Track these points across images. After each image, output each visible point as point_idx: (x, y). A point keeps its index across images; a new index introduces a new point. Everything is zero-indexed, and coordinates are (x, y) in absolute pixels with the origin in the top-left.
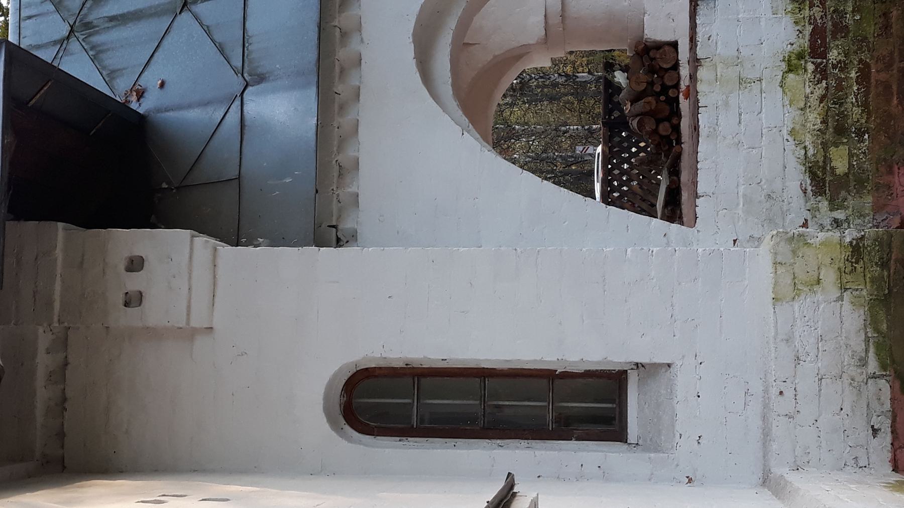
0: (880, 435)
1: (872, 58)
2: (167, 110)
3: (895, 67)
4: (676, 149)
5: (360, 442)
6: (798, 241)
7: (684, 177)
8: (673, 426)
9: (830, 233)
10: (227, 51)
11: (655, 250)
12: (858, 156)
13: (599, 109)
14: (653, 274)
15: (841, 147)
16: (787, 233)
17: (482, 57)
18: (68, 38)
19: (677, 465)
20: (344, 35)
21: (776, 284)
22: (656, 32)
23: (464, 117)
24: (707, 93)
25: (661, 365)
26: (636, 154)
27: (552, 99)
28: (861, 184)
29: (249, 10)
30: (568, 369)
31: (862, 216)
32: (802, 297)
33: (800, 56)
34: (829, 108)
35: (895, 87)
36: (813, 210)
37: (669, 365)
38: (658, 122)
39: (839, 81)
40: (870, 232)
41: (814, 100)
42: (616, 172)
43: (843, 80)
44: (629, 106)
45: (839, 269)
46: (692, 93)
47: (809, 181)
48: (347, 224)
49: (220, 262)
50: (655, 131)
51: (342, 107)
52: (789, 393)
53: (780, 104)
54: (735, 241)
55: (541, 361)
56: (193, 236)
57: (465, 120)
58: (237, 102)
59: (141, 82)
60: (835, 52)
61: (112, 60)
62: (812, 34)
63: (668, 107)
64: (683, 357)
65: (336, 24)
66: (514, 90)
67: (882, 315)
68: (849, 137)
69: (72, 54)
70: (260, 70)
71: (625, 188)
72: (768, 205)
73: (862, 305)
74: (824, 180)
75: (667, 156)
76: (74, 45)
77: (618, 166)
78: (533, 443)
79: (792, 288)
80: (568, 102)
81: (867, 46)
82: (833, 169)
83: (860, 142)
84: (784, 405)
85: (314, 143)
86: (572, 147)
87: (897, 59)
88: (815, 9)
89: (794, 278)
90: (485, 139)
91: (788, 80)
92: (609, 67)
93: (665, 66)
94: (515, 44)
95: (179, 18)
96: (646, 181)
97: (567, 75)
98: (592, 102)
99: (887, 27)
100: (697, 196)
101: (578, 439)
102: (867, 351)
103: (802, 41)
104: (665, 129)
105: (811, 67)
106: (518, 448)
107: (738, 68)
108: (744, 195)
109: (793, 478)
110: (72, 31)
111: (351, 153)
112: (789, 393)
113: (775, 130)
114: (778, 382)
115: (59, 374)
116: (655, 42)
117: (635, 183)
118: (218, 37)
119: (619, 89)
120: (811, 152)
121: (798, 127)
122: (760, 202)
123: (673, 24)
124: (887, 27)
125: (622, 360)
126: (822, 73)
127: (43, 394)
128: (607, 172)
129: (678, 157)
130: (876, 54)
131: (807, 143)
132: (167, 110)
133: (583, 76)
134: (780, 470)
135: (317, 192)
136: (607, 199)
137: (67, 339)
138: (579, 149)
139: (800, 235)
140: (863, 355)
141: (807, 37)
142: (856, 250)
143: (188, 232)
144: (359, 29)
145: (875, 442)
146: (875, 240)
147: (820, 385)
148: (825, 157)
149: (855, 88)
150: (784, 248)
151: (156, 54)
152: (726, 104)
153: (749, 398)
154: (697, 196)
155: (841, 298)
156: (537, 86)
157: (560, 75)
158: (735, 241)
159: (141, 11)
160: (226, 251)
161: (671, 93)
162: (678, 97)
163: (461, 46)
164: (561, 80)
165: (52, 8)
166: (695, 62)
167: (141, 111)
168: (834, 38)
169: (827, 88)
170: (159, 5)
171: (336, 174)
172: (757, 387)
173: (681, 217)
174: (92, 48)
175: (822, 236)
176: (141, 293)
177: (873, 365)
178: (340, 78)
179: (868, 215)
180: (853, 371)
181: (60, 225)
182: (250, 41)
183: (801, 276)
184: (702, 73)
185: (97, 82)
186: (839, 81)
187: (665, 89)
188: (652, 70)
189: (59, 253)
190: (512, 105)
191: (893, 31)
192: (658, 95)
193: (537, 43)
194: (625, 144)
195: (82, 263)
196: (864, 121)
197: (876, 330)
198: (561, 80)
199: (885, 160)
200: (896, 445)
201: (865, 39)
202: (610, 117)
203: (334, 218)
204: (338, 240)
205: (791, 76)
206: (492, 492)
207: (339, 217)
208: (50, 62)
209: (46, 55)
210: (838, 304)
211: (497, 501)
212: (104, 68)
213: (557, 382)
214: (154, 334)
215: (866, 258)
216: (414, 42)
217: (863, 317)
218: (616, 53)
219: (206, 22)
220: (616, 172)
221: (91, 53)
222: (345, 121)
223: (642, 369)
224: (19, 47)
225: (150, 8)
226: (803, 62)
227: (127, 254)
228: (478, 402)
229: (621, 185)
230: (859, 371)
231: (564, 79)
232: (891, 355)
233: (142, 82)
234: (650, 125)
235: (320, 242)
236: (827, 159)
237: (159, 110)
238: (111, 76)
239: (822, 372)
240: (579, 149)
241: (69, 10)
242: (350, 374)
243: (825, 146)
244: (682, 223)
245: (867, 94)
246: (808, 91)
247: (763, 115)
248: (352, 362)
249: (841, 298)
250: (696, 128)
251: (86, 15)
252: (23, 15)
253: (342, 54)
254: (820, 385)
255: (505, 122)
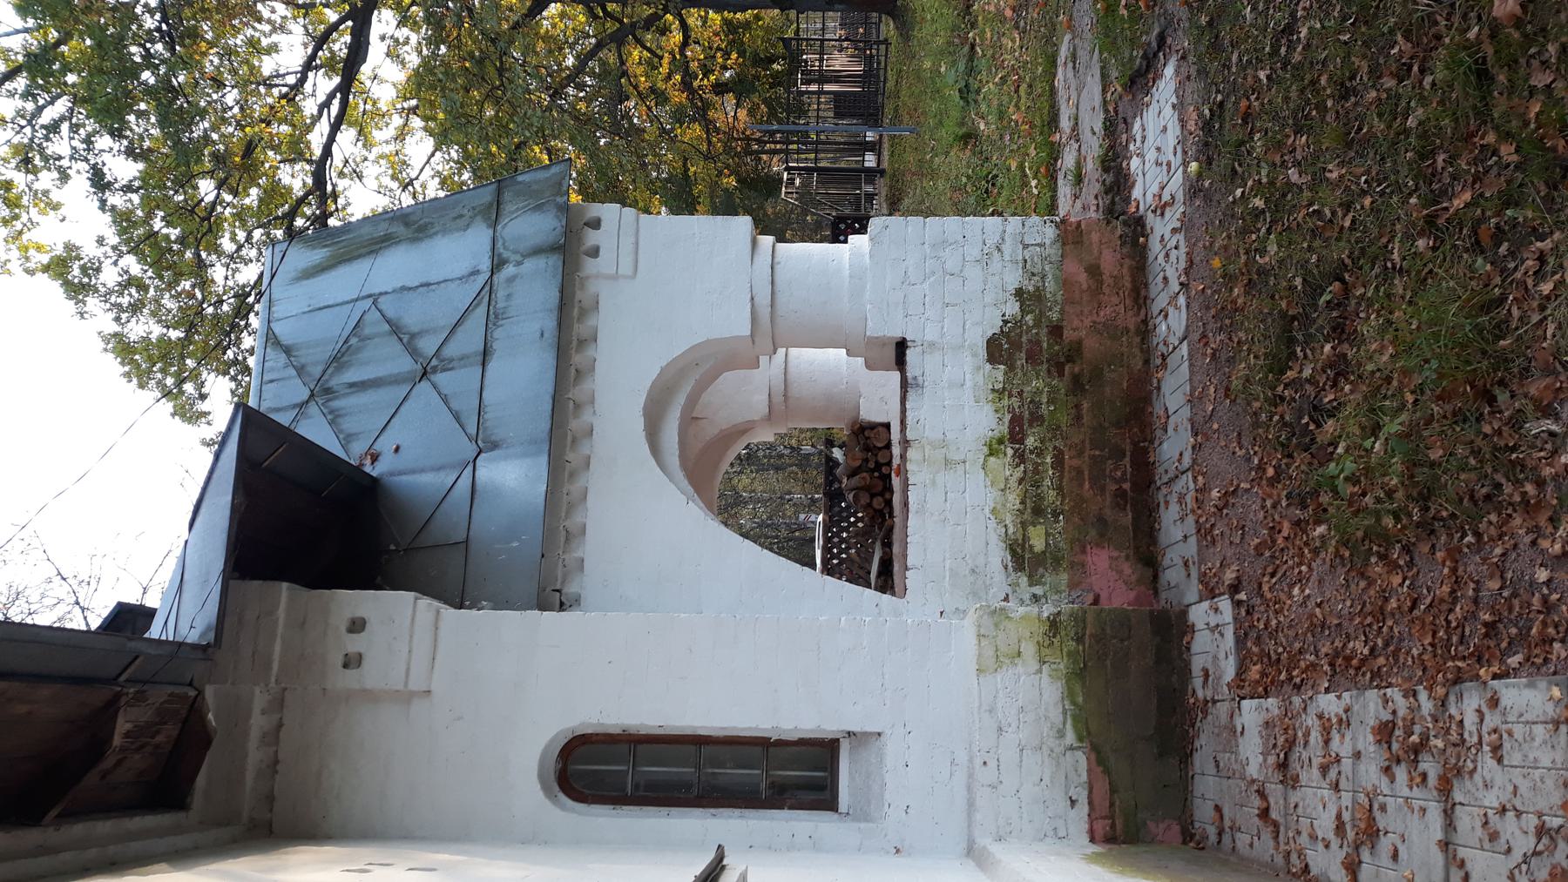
0: (1077, 806)
1: (1065, 446)
2: (401, 473)
3: (1086, 454)
4: (888, 522)
5: (573, 810)
6: (1000, 615)
7: (896, 549)
8: (883, 796)
9: (1029, 608)
10: (463, 420)
11: (867, 620)
12: (1054, 536)
13: (821, 480)
14: (864, 644)
15: (1039, 527)
16: (989, 607)
17: (710, 431)
18: (307, 402)
19: (886, 836)
20: (577, 406)
21: (980, 655)
22: (872, 412)
23: (690, 487)
24: (918, 473)
25: (871, 734)
26: (855, 524)
27: (777, 469)
28: (1057, 562)
29: (486, 382)
30: (783, 737)
31: (1058, 592)
32: (1004, 668)
33: (1000, 441)
34: (1027, 490)
35: (1086, 473)
36: (1014, 585)
37: (879, 734)
38: (873, 496)
39: (1037, 465)
40: (1066, 607)
41: (1013, 483)
42: (836, 540)
43: (1039, 464)
44: (845, 480)
45: (1038, 642)
46: (902, 471)
47: (1009, 558)
48: (571, 589)
49: (443, 626)
50: (869, 505)
51: (572, 475)
52: (992, 764)
53: (982, 484)
54: (942, 613)
55: (756, 729)
56: (416, 599)
57: (690, 489)
58: (470, 468)
59: (374, 447)
60: (1032, 439)
61: (348, 425)
62: (1011, 421)
63: (881, 483)
64: (893, 726)
65: (570, 396)
66: (741, 460)
67: (1078, 688)
68: (1045, 517)
69: (310, 417)
70: (493, 438)
71: (844, 556)
72: (972, 579)
73: (1059, 678)
74: (1023, 557)
75: (880, 529)
76: (313, 409)
77: (837, 534)
78: (747, 812)
79: (994, 660)
80: (792, 472)
81: (1061, 434)
82: (1031, 547)
83: (1058, 522)
84: (985, 776)
85: (542, 508)
86: (796, 513)
87: (1088, 446)
88: (1014, 399)
89: (997, 651)
90: (709, 506)
91: (989, 463)
92: (830, 443)
93: (880, 445)
94: (740, 420)
95: (418, 386)
96: (863, 549)
97: (792, 448)
98: (815, 473)
99: (1078, 417)
100: (907, 569)
101: (790, 808)
102: (1064, 724)
103: (1001, 428)
104: (878, 503)
105: (1010, 452)
106: (730, 817)
107: (944, 450)
108: (951, 570)
109: (996, 849)
110: (312, 395)
111: (577, 518)
112: (992, 764)
113: (978, 509)
114: (982, 752)
115: (273, 736)
116: (869, 422)
117: (853, 551)
118: (455, 405)
119: (837, 464)
120: (1011, 531)
121: (999, 507)
122: (965, 576)
123: (886, 407)
124: (1078, 417)
125: (834, 729)
126: (1020, 457)
127: (255, 755)
128: (827, 540)
129: (891, 529)
130: (1069, 442)
131: (1007, 522)
132: (401, 473)
133: (807, 449)
134: (985, 841)
135: (543, 556)
136: (828, 570)
137: (283, 700)
138: (802, 516)
139: (1002, 609)
140: (1061, 727)
141: (1007, 424)
142: (1054, 624)
143: (412, 594)
144: (592, 401)
145: (1072, 813)
146: (1071, 616)
147: (1021, 756)
148: (1024, 535)
149: (1051, 473)
150: (988, 622)
151: (402, 409)
152: (934, 483)
153: (954, 768)
154: (907, 569)
155: (1040, 671)
156: (765, 457)
157: (785, 447)
158: (942, 613)
159: (380, 378)
160: (449, 613)
161: (884, 470)
162: (890, 474)
163: (690, 420)
164: (787, 452)
165: (294, 372)
166: (905, 443)
167: (374, 474)
168: (1031, 426)
169: (1025, 472)
170: (399, 374)
171: (563, 539)
172: (962, 757)
173: (892, 587)
174: (330, 413)
175: (1022, 610)
176: (360, 655)
177: (1070, 738)
178: (572, 447)
179: (1064, 591)
180: (1052, 742)
181: (285, 585)
182: (486, 410)
183: (1003, 648)
184: (911, 454)
185: (334, 447)
186: (1037, 465)
187: (878, 466)
188: (867, 449)
189: (281, 613)
190: (741, 472)
191: (1084, 421)
192: (873, 471)
193: (762, 420)
194: (845, 514)
195: (304, 623)
196: (1058, 503)
197: (1073, 703)
198: (787, 452)
199: (1078, 540)
200: (1093, 816)
201: (1059, 427)
202: (831, 487)
203: (559, 582)
204: (562, 604)
205: (992, 459)
206: (699, 867)
207: (563, 582)
208: (287, 425)
209: (284, 419)
210: (1038, 677)
211: (704, 876)
212: (341, 431)
213: (771, 749)
214: (371, 697)
215: (1063, 633)
216: (644, 415)
217: (1061, 690)
218: (834, 431)
219: (444, 391)
220: (836, 540)
221: (329, 417)
222: (575, 488)
223: (853, 737)
224: (258, 412)
225: (390, 376)
226: (1002, 447)
227: (350, 616)
228: (693, 770)
229: (840, 553)
230: (1057, 742)
231: (789, 451)
232: (1087, 728)
233: (377, 447)
234: (865, 499)
235: (543, 606)
236: (1025, 538)
237: (392, 474)
238: (347, 440)
239: (1023, 743)
240: (802, 516)
241: (310, 375)
242: (566, 741)
243: (1024, 525)
244: (893, 594)
245: (1061, 478)
246: (1008, 473)
247: (967, 495)
248: (568, 729)
249: (1040, 671)
250: (906, 504)
251: (327, 381)
252: (265, 378)
253: (574, 425)
254: (1021, 756)
255: (734, 489)
